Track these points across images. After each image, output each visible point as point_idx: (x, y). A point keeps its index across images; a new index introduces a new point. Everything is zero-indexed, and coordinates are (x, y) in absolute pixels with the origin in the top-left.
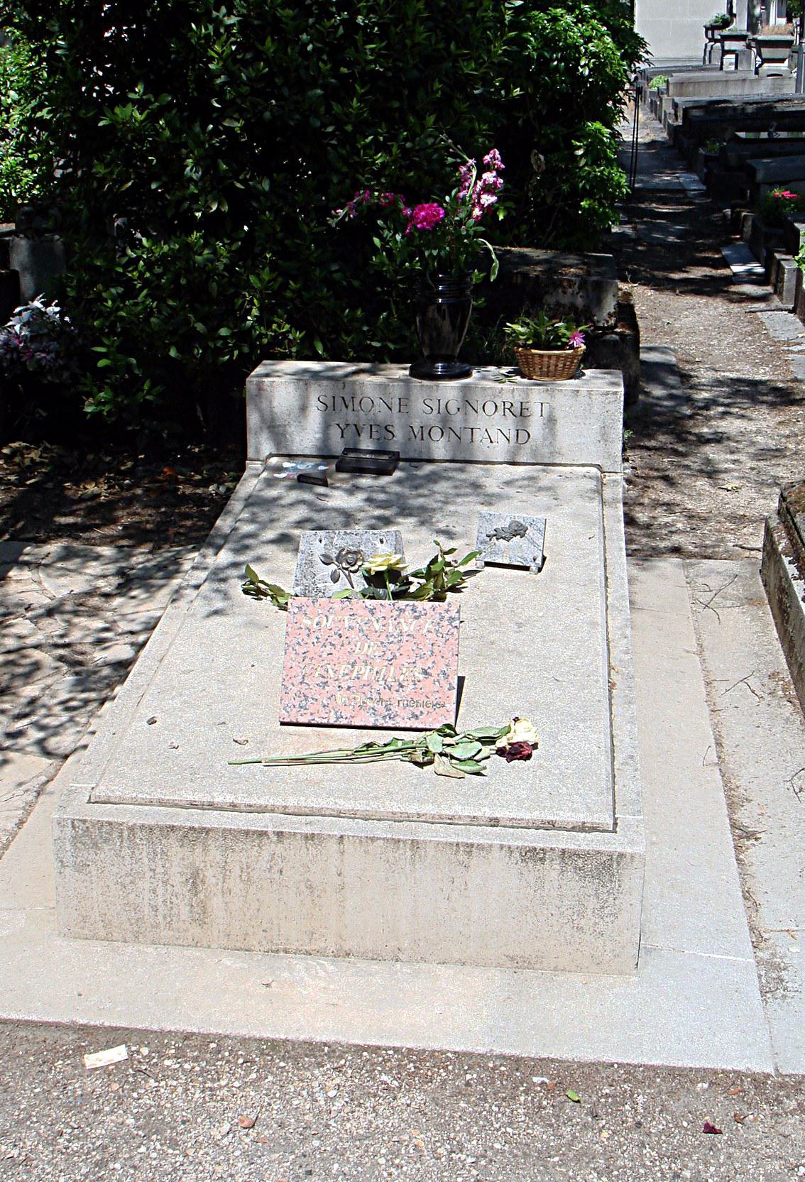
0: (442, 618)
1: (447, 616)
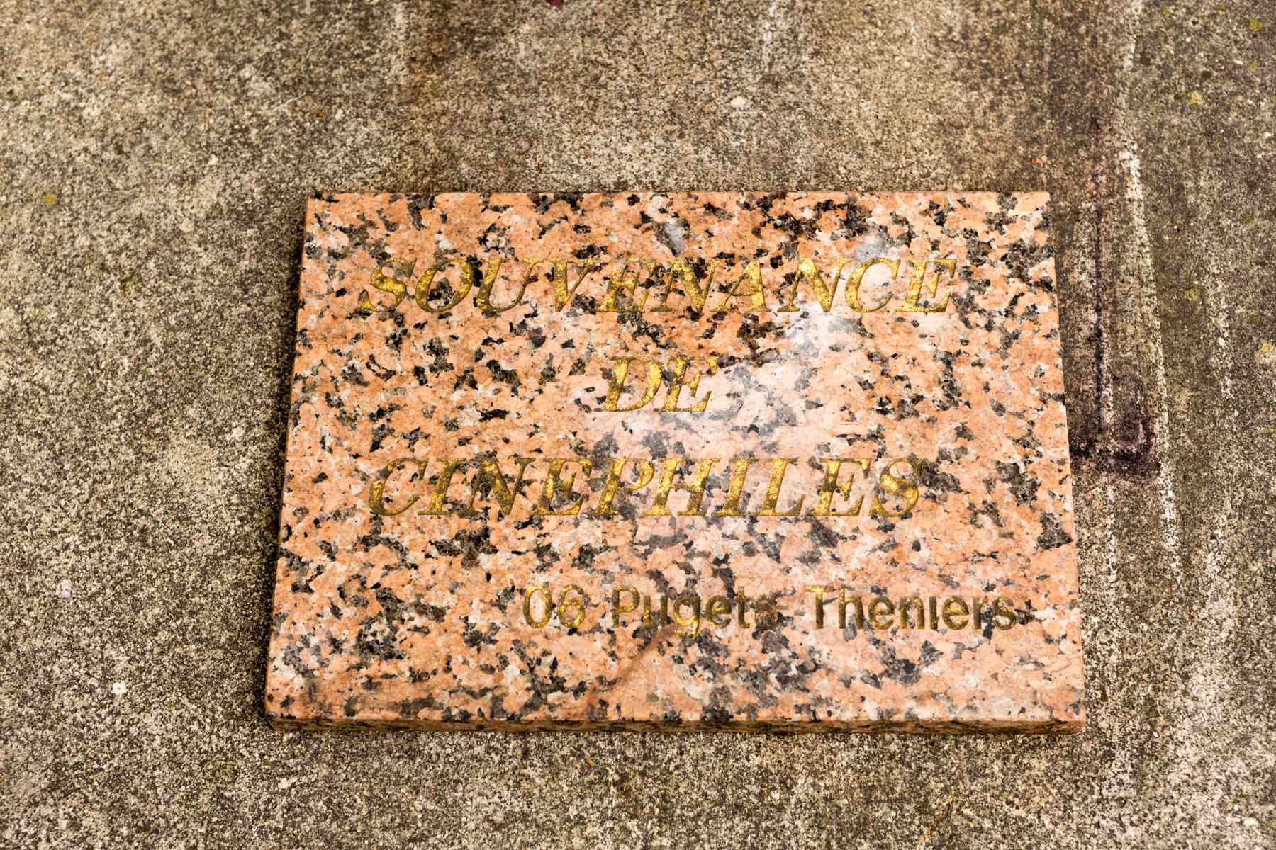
0: (979, 252)
1: (1000, 243)
